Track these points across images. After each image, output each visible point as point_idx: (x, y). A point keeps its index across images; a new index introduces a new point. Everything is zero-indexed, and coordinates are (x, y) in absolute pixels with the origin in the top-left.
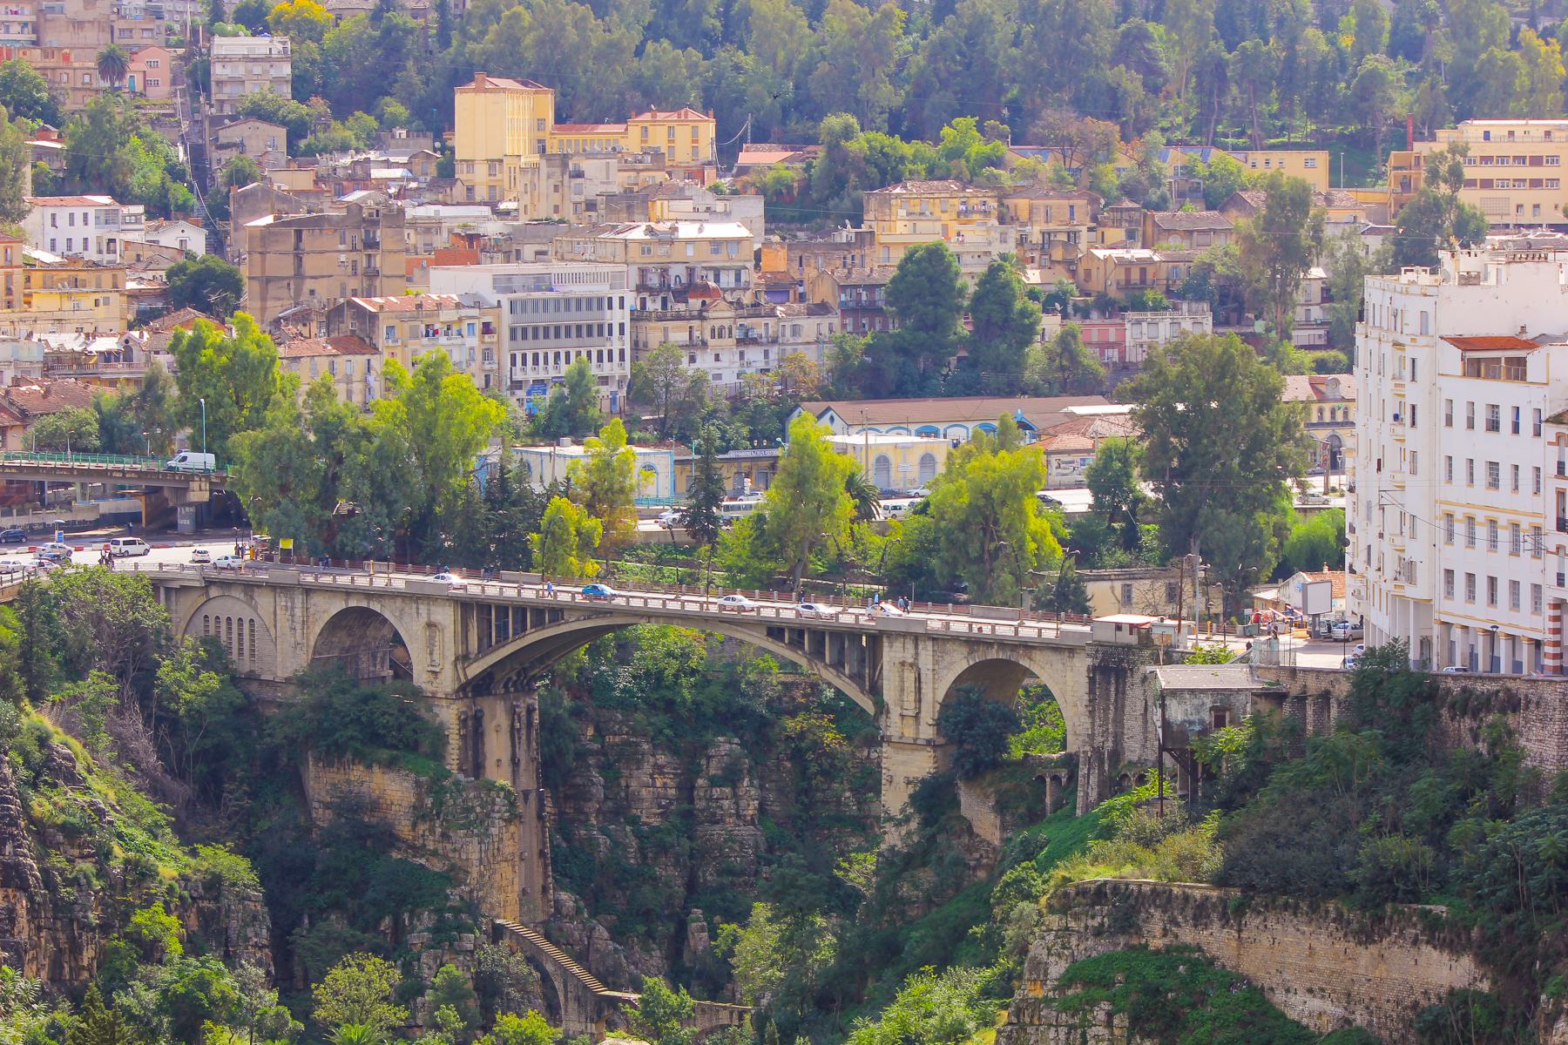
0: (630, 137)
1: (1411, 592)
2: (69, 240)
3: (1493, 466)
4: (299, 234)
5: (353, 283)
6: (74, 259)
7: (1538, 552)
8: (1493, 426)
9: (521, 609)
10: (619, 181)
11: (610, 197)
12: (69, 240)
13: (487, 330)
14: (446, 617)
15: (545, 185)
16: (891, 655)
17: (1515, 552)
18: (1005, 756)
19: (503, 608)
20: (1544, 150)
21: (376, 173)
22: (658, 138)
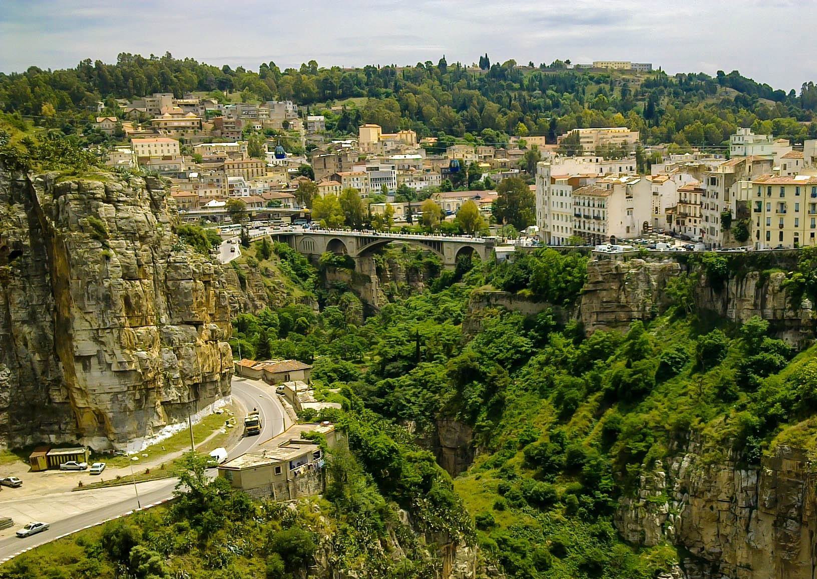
0: (397, 137)
1: (546, 230)
2: (797, 194)
3: (562, 203)
4: (759, 188)
5: (337, 170)
6: (276, 166)
7: (571, 221)
8: (562, 195)
9: (369, 238)
10: (394, 146)
11: (393, 150)
12: (797, 194)
13: (366, 179)
14: (354, 240)
15: (379, 148)
16: (445, 245)
17: (567, 221)
18: (805, 294)
19: (365, 238)
20: (590, 135)
21: (343, 146)
22: (404, 136)
